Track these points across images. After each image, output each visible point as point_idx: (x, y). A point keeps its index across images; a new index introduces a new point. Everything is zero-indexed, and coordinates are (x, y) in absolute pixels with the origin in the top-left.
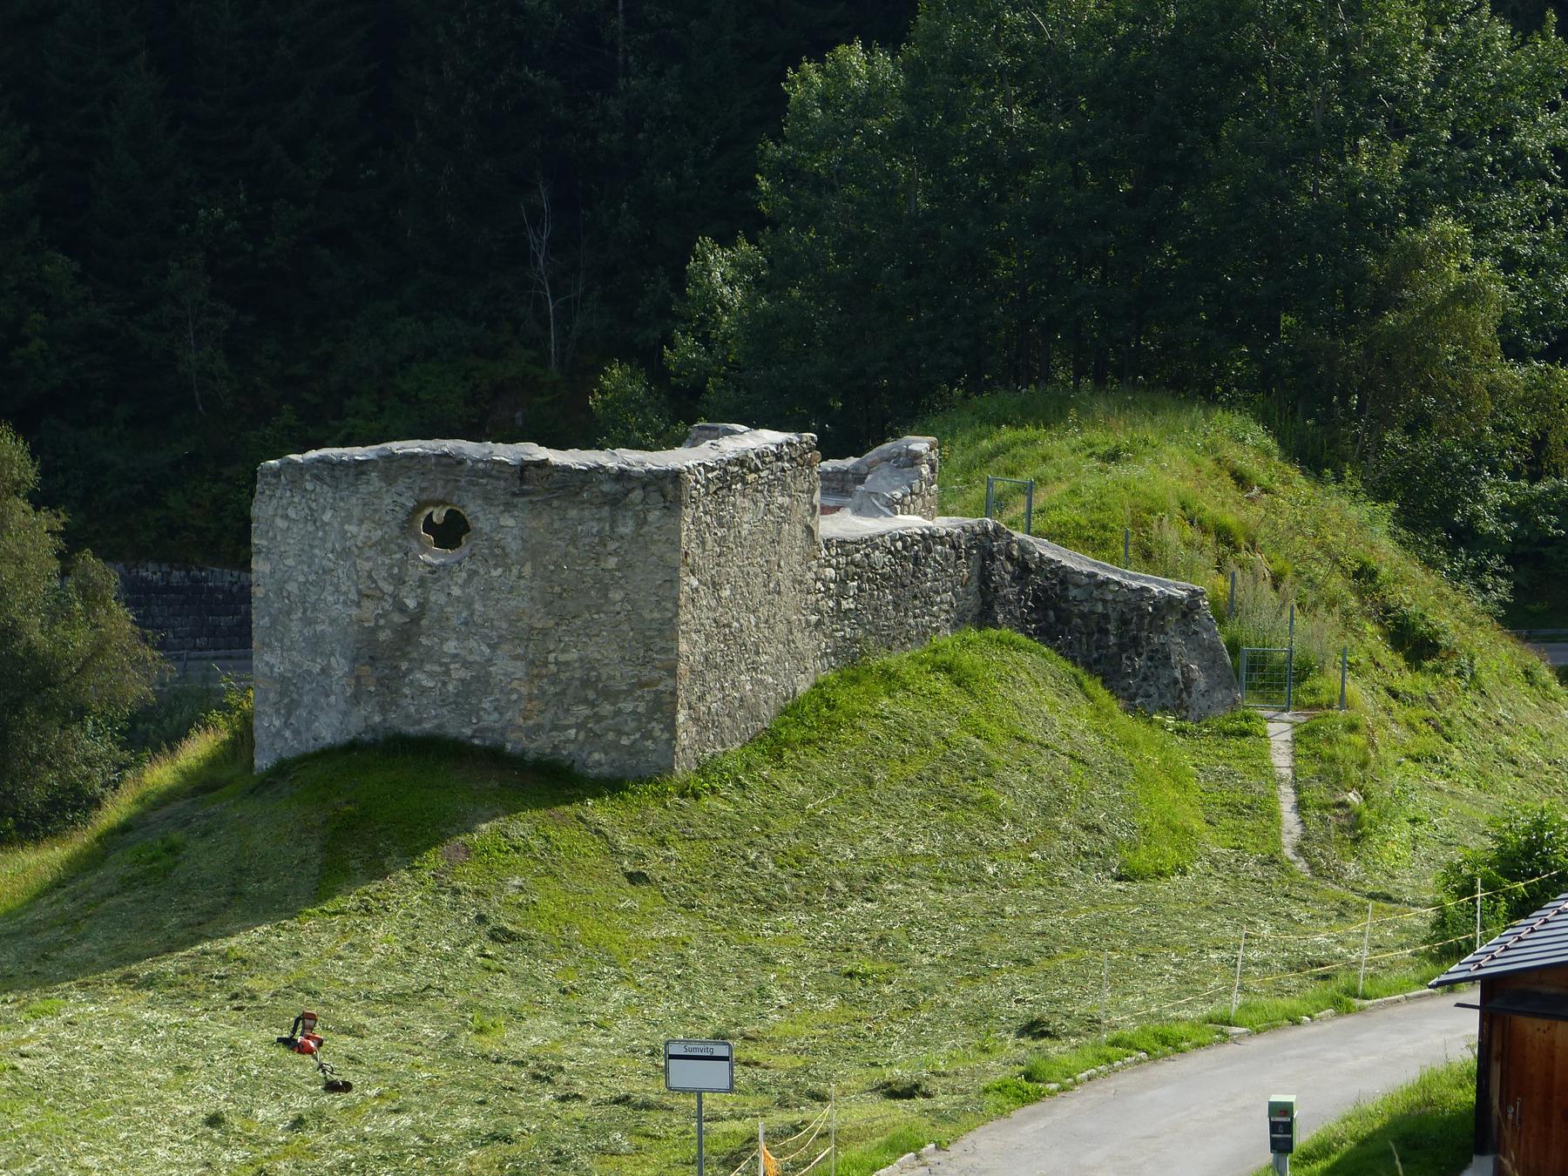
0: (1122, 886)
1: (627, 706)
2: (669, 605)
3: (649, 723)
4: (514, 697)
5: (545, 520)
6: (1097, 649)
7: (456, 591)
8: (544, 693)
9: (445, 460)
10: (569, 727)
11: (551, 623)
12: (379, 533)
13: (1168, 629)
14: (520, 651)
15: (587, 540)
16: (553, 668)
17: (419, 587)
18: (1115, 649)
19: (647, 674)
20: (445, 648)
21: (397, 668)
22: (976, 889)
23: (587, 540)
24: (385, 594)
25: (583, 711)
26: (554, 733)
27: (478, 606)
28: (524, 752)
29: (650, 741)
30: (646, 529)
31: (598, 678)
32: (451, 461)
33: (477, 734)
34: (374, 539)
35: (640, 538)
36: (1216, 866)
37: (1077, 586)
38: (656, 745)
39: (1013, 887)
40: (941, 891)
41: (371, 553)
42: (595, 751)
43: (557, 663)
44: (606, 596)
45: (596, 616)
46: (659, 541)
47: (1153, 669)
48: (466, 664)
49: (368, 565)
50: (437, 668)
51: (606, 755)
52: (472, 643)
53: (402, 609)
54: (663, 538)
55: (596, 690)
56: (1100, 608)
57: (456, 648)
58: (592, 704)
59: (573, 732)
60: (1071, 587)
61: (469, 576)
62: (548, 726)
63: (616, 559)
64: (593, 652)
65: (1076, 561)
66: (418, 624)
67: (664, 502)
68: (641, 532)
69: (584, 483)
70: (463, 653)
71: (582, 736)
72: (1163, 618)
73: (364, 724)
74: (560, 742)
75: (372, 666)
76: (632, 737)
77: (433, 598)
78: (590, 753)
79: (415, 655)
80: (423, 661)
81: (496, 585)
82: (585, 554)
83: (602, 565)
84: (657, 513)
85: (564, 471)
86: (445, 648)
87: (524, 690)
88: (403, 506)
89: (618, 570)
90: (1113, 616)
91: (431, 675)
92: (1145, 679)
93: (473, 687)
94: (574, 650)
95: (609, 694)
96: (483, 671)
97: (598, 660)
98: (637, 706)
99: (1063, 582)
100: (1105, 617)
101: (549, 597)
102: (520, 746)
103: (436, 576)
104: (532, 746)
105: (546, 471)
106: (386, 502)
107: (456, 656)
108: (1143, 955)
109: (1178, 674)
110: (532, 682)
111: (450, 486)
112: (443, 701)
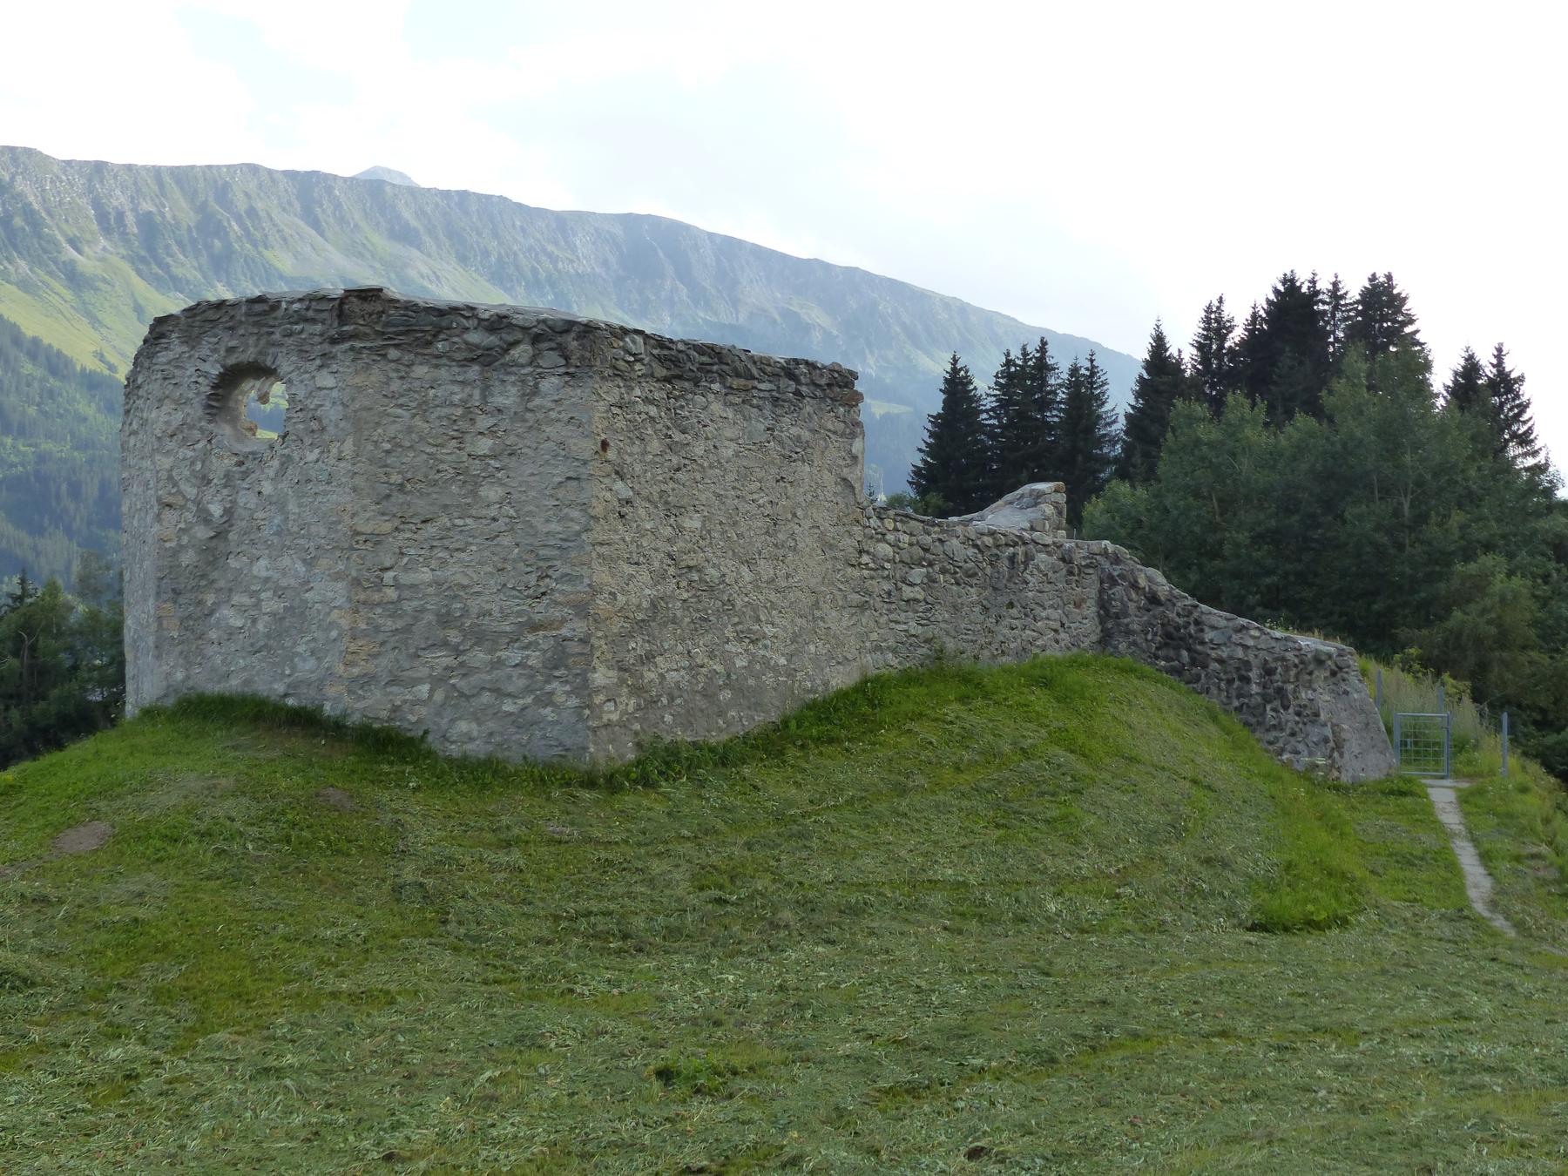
0: (1252, 937)
1: (514, 656)
2: (575, 514)
3: (548, 682)
4: (334, 634)
5: (375, 376)
7: (267, 488)
8: (377, 629)
9: (259, 308)
10: (419, 681)
11: (387, 527)
12: (180, 416)
13: (1315, 686)
14: (341, 566)
15: (445, 411)
16: (392, 594)
17: (225, 486)
18: (1259, 699)
19: (541, 611)
20: (255, 570)
21: (200, 603)
22: (1020, 932)
23: (445, 411)
24: (188, 500)
25: (443, 659)
26: (394, 689)
27: (292, 507)
28: (345, 715)
29: (549, 709)
30: (537, 401)
31: (465, 612)
32: (265, 307)
33: (291, 691)
34: (175, 424)
35: (529, 415)
36: (1387, 921)
37: (1214, 628)
38: (558, 714)
39: (1083, 931)
40: (960, 932)
41: (171, 445)
42: (460, 718)
43: (397, 586)
44: (474, 493)
45: (459, 522)
46: (558, 420)
47: (1300, 725)
48: (280, 593)
49: (166, 462)
50: (246, 600)
51: (479, 725)
52: (286, 561)
53: (206, 519)
54: (565, 416)
55: (461, 629)
56: (1240, 653)
57: (268, 569)
58: (457, 651)
59: (425, 688)
60: (1207, 629)
61: (282, 464)
62: (385, 678)
63: (490, 442)
64: (454, 573)
66: (226, 539)
67: (567, 365)
68: (530, 405)
69: (440, 330)
70: (276, 576)
71: (439, 696)
72: (1311, 673)
73: (164, 683)
74: (405, 702)
75: (175, 602)
76: (521, 702)
77: (241, 501)
78: (453, 721)
79: (222, 584)
80: (230, 590)
81: (313, 474)
82: (441, 430)
83: (469, 449)
84: (554, 380)
85: (406, 308)
86: (255, 570)
87: (345, 623)
88: (206, 375)
89: (494, 457)
90: (1255, 662)
91: (241, 609)
92: (1293, 734)
93: (287, 623)
94: (425, 569)
95: (480, 637)
96: (297, 599)
97: (464, 587)
98: (528, 657)
100: (1247, 665)
101: (384, 490)
102: (341, 706)
103: (243, 468)
104: (359, 705)
106: (188, 373)
107: (267, 580)
108: (1279, 1049)
109: (1328, 732)
110: (357, 612)
111: (262, 342)
112: (252, 645)
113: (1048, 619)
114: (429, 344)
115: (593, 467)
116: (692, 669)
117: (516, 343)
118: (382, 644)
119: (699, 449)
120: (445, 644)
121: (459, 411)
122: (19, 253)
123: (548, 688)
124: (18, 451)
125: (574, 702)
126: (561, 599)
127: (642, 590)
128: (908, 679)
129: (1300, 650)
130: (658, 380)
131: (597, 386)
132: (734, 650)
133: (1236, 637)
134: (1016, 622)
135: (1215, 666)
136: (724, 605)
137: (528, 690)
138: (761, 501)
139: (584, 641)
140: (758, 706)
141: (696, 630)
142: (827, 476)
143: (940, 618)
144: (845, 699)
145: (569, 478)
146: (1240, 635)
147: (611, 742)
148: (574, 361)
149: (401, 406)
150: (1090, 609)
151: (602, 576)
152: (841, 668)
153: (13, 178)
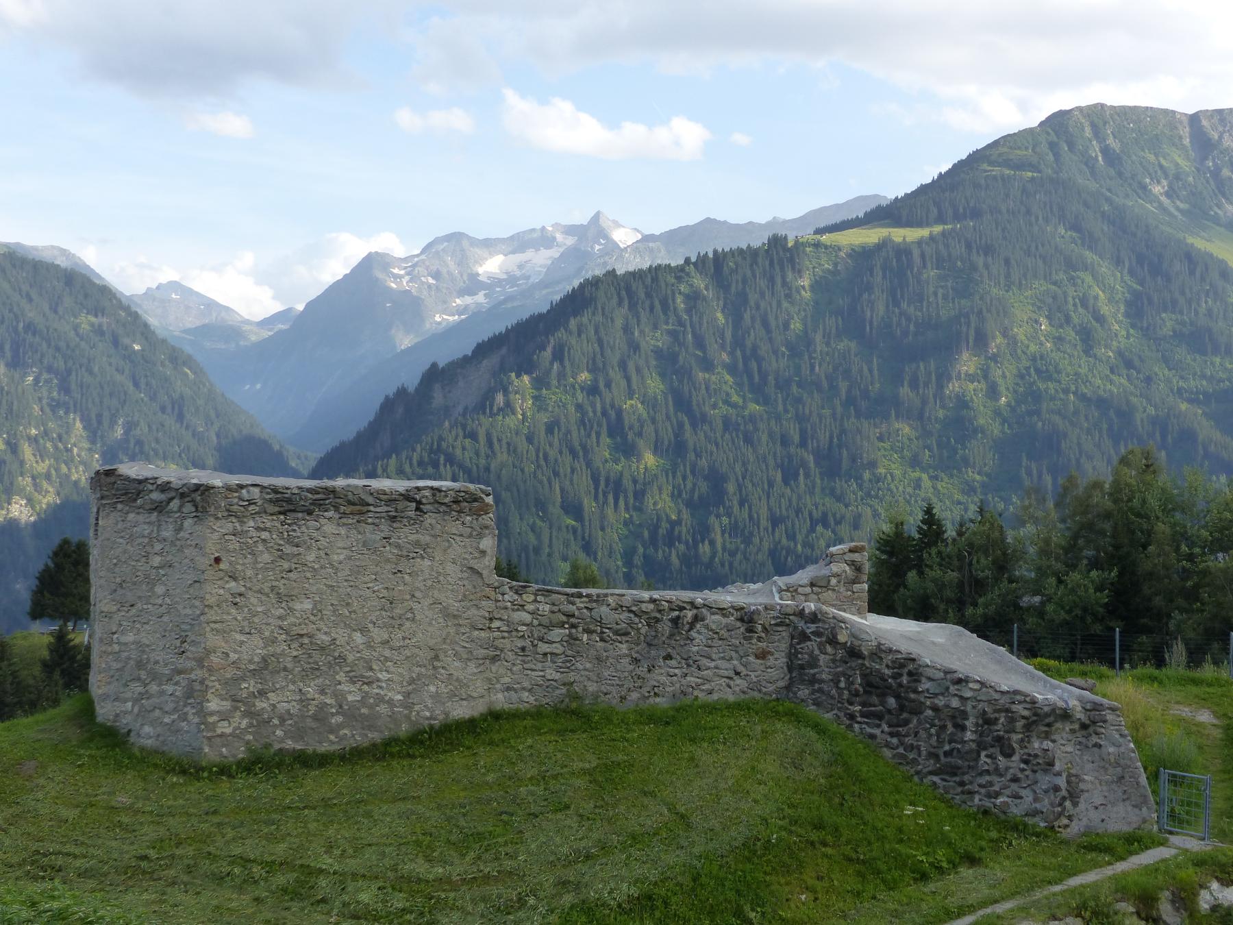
1: (169, 688)
2: (197, 603)
6: (950, 743)
15: (140, 540)
16: (116, 648)
18: (974, 746)
19: (182, 663)
25: (137, 688)
30: (182, 534)
35: (178, 542)
37: (930, 679)
45: (145, 607)
54: (193, 543)
56: (955, 703)
60: (924, 680)
65: (1056, 682)
68: (179, 536)
71: (136, 710)
78: (142, 725)
84: (190, 521)
85: (125, 480)
95: (154, 677)
99: (915, 676)
101: (113, 586)
105: (112, 479)
109: (1062, 782)
113: (716, 668)
114: (135, 500)
115: (210, 574)
116: (303, 701)
117: (172, 499)
118: (112, 677)
119: (311, 557)
120: (139, 679)
121: (146, 540)
122: (1227, 199)
123: (186, 710)
124: (1226, 369)
125: (196, 720)
126: (191, 656)
127: (254, 649)
128: (537, 714)
129: (1035, 703)
130: (272, 515)
131: (211, 524)
132: (346, 689)
133: (953, 689)
134: (676, 671)
135: (929, 712)
136: (335, 659)
137: (175, 710)
138: (376, 588)
139: (202, 682)
140: (371, 727)
141: (307, 675)
142: (450, 568)
143: (581, 667)
144: (470, 726)
145: (196, 582)
146: (956, 687)
147: (223, 746)
148: (200, 509)
149: (122, 537)
150: (779, 659)
151: (213, 640)
152: (465, 703)
153: (1221, 137)
